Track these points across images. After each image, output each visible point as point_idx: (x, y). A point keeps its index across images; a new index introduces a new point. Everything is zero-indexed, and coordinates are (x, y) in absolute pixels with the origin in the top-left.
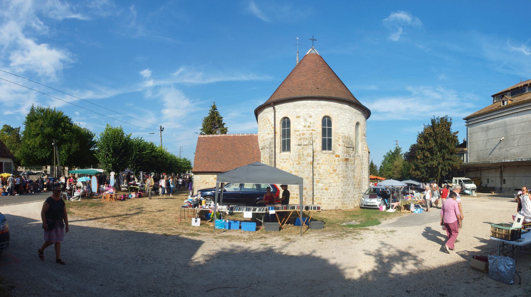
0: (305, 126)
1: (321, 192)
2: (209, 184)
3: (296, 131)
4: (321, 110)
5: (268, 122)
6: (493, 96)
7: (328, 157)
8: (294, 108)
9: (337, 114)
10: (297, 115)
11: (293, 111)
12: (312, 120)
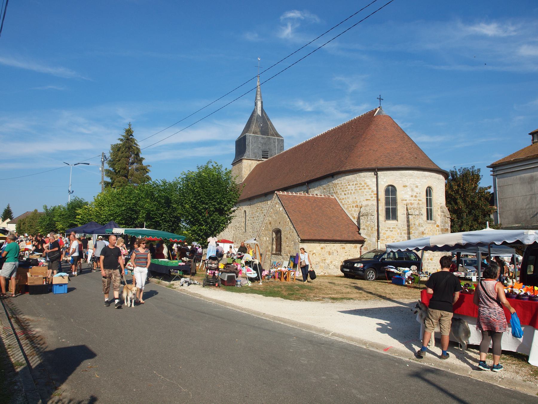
0: (412, 196)
2: (316, 255)
3: (403, 200)
4: (425, 180)
5: (367, 188)
6: (532, 134)
7: (432, 227)
9: (436, 184)
12: (418, 190)
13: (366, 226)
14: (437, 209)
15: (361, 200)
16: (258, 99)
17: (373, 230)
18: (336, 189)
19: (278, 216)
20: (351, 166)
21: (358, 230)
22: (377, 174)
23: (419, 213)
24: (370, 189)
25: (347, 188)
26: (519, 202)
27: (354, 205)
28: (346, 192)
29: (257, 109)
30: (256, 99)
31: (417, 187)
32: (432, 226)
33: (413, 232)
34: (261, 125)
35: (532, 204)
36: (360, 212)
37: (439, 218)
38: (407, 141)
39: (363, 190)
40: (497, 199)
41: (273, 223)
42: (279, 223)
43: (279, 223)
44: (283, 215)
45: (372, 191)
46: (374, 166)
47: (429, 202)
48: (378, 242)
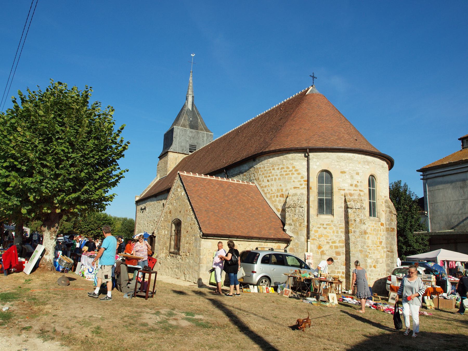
0: (351, 185)
1: (370, 270)
3: (341, 190)
4: (368, 167)
5: (295, 173)
6: (462, 139)
7: (375, 226)
8: (338, 160)
9: (380, 173)
11: (336, 164)
12: (359, 178)
13: (293, 221)
14: (381, 203)
15: (288, 187)
17: (302, 226)
19: (179, 203)
20: (276, 146)
21: (282, 226)
22: (309, 155)
23: (361, 207)
24: (299, 174)
25: (271, 172)
27: (279, 194)
28: (269, 179)
29: (188, 103)
30: (187, 94)
31: (358, 174)
32: (375, 224)
33: (353, 230)
34: (191, 119)
35: (465, 209)
36: (286, 202)
38: (344, 122)
40: (427, 204)
41: (173, 211)
42: (180, 212)
43: (180, 212)
44: (184, 201)
45: (302, 177)
46: (304, 145)
47: (372, 194)
48: (307, 241)
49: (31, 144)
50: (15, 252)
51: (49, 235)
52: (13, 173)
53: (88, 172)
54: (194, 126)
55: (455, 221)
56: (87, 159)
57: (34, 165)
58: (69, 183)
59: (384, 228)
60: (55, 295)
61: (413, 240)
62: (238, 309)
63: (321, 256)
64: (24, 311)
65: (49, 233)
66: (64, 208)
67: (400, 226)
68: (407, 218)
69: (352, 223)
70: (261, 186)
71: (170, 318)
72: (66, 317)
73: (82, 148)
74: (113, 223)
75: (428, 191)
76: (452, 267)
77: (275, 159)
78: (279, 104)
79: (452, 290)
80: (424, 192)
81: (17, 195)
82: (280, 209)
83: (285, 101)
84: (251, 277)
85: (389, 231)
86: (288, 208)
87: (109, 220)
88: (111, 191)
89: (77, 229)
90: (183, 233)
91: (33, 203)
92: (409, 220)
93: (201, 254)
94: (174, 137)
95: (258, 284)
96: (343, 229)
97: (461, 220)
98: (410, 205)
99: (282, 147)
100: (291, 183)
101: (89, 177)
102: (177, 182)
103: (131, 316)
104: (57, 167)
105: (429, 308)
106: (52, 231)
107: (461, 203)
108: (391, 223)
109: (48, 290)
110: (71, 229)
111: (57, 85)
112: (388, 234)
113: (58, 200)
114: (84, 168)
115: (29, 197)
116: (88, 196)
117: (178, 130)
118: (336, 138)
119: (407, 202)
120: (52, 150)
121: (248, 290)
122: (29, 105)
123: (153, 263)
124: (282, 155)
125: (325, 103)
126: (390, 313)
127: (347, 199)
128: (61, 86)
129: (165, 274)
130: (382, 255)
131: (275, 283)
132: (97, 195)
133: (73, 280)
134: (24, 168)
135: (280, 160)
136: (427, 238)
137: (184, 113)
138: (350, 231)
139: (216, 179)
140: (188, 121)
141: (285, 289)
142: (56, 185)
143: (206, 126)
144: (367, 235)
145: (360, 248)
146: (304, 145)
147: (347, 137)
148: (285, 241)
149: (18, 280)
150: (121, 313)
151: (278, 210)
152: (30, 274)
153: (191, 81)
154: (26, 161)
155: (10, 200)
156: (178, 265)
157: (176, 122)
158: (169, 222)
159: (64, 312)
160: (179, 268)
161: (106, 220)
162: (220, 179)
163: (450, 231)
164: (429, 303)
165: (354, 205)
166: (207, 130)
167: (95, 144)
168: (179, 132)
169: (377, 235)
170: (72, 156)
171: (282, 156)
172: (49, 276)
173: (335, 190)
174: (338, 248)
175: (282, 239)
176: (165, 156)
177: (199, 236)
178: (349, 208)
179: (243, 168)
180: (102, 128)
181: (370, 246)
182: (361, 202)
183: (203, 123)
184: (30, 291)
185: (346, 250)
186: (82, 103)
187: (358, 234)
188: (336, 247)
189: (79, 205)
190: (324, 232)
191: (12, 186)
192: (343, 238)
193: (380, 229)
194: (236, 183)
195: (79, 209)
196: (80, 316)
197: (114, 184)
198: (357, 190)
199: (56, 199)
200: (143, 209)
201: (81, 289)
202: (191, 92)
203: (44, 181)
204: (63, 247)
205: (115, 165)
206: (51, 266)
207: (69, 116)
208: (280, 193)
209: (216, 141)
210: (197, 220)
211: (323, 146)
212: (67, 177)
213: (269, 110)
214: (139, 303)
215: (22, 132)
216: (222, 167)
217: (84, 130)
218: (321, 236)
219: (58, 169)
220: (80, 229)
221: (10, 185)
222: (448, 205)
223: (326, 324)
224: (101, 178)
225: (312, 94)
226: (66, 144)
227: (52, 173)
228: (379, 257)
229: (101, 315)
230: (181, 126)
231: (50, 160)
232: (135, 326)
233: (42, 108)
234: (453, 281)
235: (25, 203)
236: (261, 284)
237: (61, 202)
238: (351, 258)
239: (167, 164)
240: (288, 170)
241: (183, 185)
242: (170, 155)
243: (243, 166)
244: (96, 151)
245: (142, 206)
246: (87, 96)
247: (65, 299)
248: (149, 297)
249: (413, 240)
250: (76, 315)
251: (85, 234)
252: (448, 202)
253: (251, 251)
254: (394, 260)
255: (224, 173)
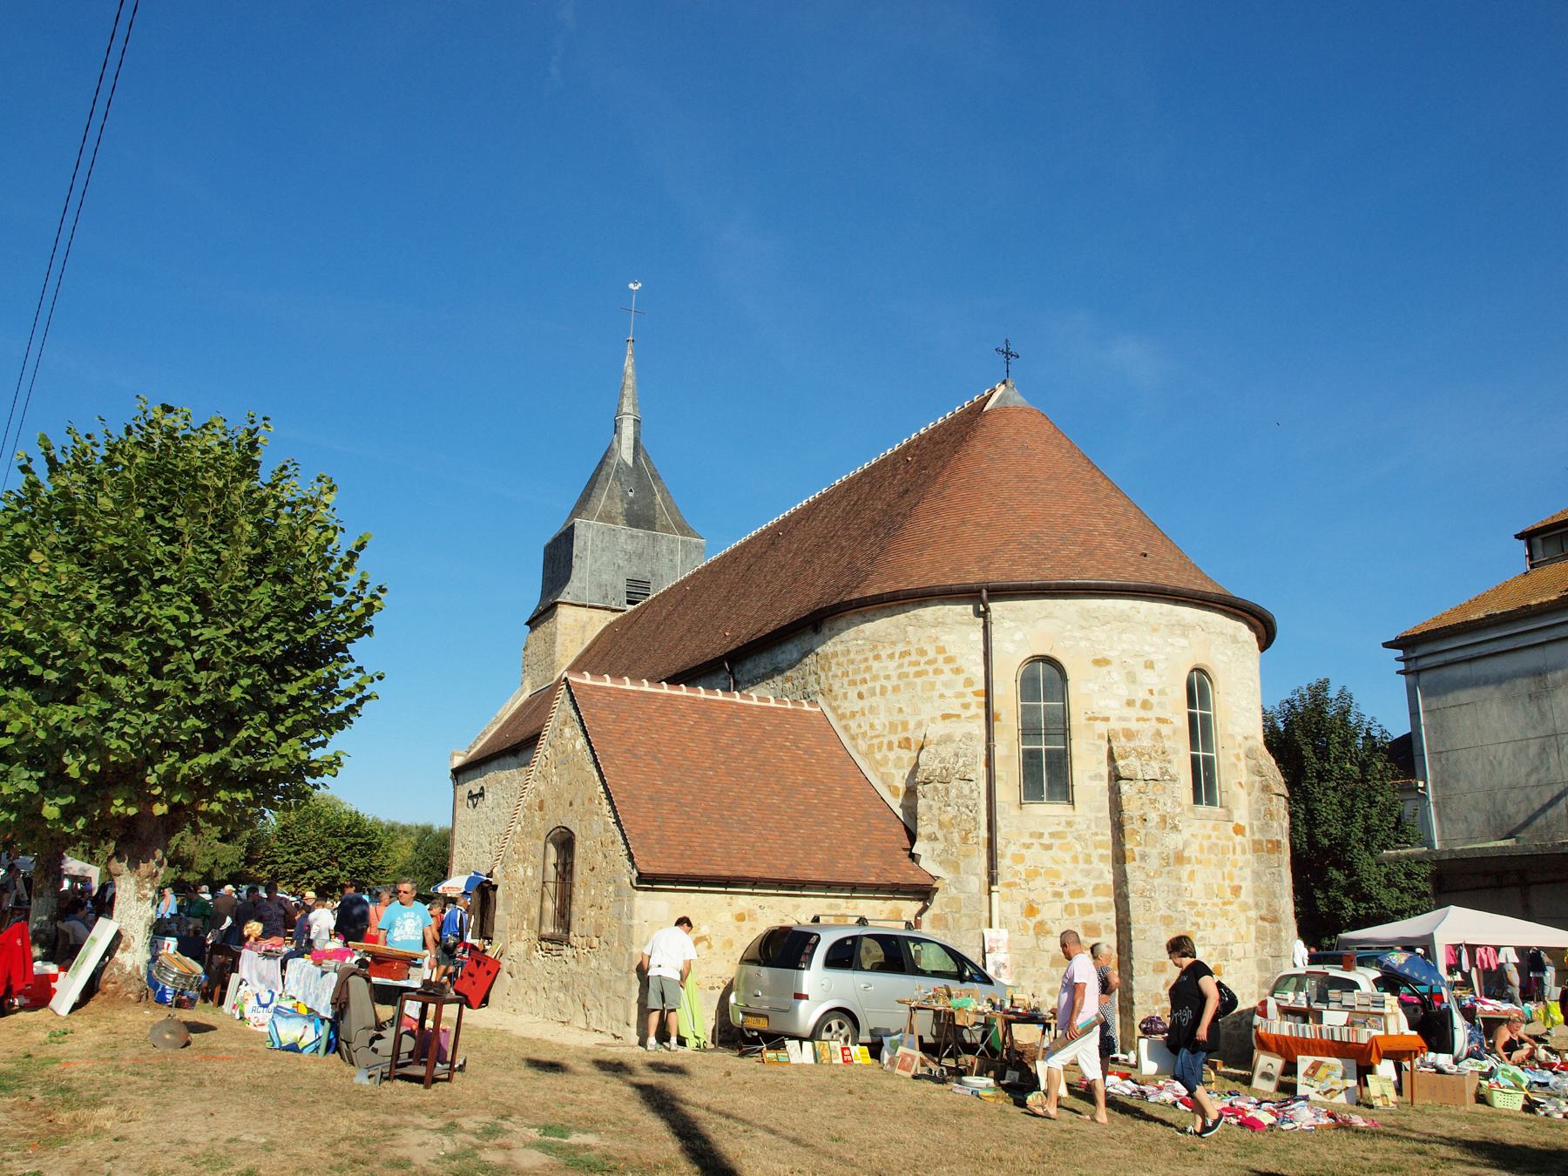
0: (1130, 703)
2: (710, 947)
3: (1096, 719)
4: (1183, 642)
5: (947, 668)
6: (1527, 536)
7: (1214, 834)
10: (1095, 655)
11: (1078, 635)
13: (941, 825)
14: (1233, 759)
15: (924, 717)
16: (625, 410)
17: (970, 842)
18: (827, 679)
21: (906, 843)
22: (987, 610)
23: (1163, 774)
24: (958, 671)
25: (868, 669)
26: (1500, 764)
27: (895, 739)
28: (863, 688)
30: (619, 412)
31: (1150, 665)
32: (1215, 828)
33: (1137, 850)
34: (631, 494)
35: (1548, 769)
36: (917, 765)
37: (1242, 794)
38: (1106, 497)
39: (931, 677)
40: (1423, 755)
41: (549, 803)
42: (571, 804)
43: (571, 804)
44: (582, 769)
45: (969, 682)
46: (974, 577)
47: (1200, 730)
48: (990, 892)
49: (73, 600)
50: (22, 942)
51: (134, 888)
52: (18, 693)
53: (253, 685)
54: (640, 518)
55: (1518, 813)
56: (250, 643)
57: (84, 666)
58: (192, 721)
59: (1244, 840)
60: (135, 1078)
61: (1375, 879)
62: (720, 1114)
63: (1037, 939)
64: (30, 1126)
65: (132, 881)
66: (176, 799)
67: (1332, 830)
68: (1353, 805)
69: (1136, 827)
70: (838, 715)
71: (486, 1144)
72: (154, 1143)
73: (231, 612)
74: (380, 845)
75: (1424, 712)
76: (1486, 966)
77: (880, 626)
78: (905, 442)
79: (1469, 1042)
80: (1411, 714)
81: (32, 762)
82: (901, 786)
83: (922, 431)
84: (791, 1012)
85: (1263, 851)
86: (925, 783)
87: (368, 834)
88: (339, 741)
89: (261, 867)
90: (579, 873)
91: (81, 784)
92: (1358, 812)
93: (635, 940)
94: (574, 554)
95: (814, 1036)
96: (1106, 849)
97: (1537, 806)
98: (1364, 760)
99: (903, 586)
100: (932, 702)
101: (257, 699)
102: (563, 707)
103: (361, 1139)
104: (155, 670)
105: (1378, 1103)
106: (142, 874)
107: (1533, 749)
108: (1267, 824)
109: (115, 1063)
110: (237, 865)
111: (156, 413)
112: (1259, 860)
113: (159, 776)
114: (242, 672)
115: (66, 766)
116: (253, 761)
117: (587, 532)
118: (1077, 549)
119: (1349, 751)
120: (140, 617)
121: (781, 1055)
122: (75, 482)
123: (488, 973)
124: (904, 612)
125: (1044, 438)
126: (1234, 1121)
127: (1115, 748)
128: (173, 417)
129: (526, 1009)
130: (1243, 929)
131: (872, 1032)
132: (282, 756)
133: (206, 1031)
134: (52, 676)
135: (897, 627)
136: (1426, 870)
137: (608, 474)
138: (1128, 854)
139: (689, 694)
140: (622, 501)
141: (901, 1049)
142: (150, 726)
143: (681, 516)
144: (1188, 867)
145: (1164, 911)
146: (974, 576)
147: (1115, 545)
148: (915, 892)
149: (27, 1032)
150: (332, 1129)
151: (894, 791)
152: (70, 1013)
153: (630, 371)
154: (59, 653)
155: (6, 776)
156: (565, 980)
157: (583, 504)
158: (538, 838)
159: (150, 1126)
160: (567, 990)
161: (358, 835)
162: (702, 693)
163: (1502, 843)
164: (1379, 1087)
165: (1139, 768)
166: (684, 529)
167: (278, 597)
168: (593, 540)
169: (1221, 865)
170: (201, 634)
171: (903, 615)
172: (130, 1018)
173: (1077, 720)
174: (1090, 912)
175: (905, 885)
176: (547, 619)
177: (628, 881)
178: (1121, 779)
179: (783, 656)
180: (299, 546)
181: (1200, 902)
182: (1161, 757)
183: (672, 509)
184: (57, 1065)
185: (1117, 916)
186: (235, 469)
187: (1154, 863)
188: (1087, 909)
189: (225, 790)
190: (1046, 859)
191: (12, 734)
192: (1109, 878)
193: (1231, 843)
194: (757, 706)
195: (226, 801)
196: (201, 1139)
197: (341, 721)
198: (1148, 720)
199: (154, 771)
200: (476, 796)
201: (223, 1059)
202: (631, 407)
203: (115, 716)
204: (191, 927)
205: (342, 660)
206: (139, 985)
207: (191, 512)
208: (898, 736)
209: (709, 565)
210: (622, 831)
211: (1034, 577)
212: (185, 703)
213: (873, 462)
214: (399, 1099)
215: (45, 564)
216: (718, 654)
217: (237, 557)
218: (1033, 874)
219: (159, 676)
220: (269, 867)
221: (8, 730)
222: (1491, 758)
223: (1000, 1160)
224: (295, 701)
225: (1002, 411)
226: (182, 600)
227: (138, 689)
228: (1231, 939)
229: (267, 1134)
230: (600, 519)
231: (133, 650)
232: (369, 1168)
233: (108, 490)
234: (1490, 1012)
235: (56, 787)
236: (825, 1035)
237: (168, 781)
238: (1133, 943)
239: (554, 643)
240: (923, 660)
241: (580, 717)
242: (564, 613)
243: (784, 648)
244: (278, 617)
245: (474, 785)
246: (253, 446)
247: (163, 1090)
248: (435, 1080)
249: (1375, 879)
250: (189, 1137)
251: (287, 883)
252: (1492, 748)
253: (794, 929)
254: (1284, 946)
255: (726, 674)
